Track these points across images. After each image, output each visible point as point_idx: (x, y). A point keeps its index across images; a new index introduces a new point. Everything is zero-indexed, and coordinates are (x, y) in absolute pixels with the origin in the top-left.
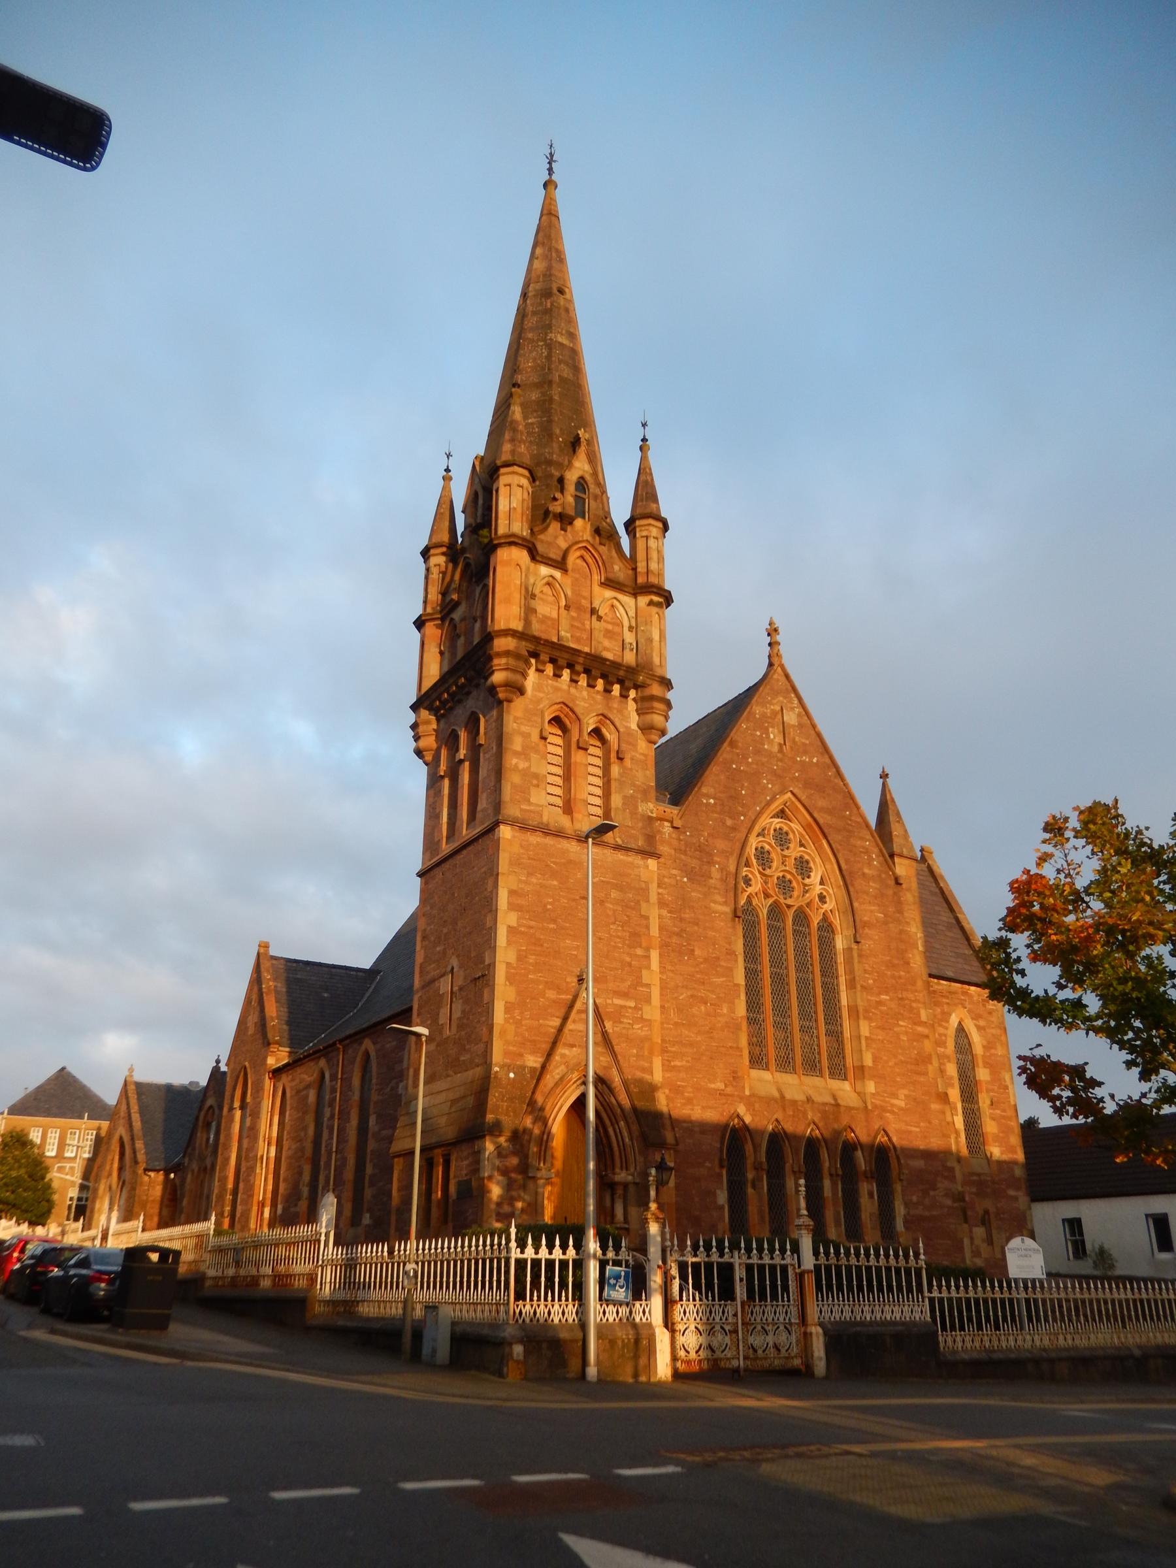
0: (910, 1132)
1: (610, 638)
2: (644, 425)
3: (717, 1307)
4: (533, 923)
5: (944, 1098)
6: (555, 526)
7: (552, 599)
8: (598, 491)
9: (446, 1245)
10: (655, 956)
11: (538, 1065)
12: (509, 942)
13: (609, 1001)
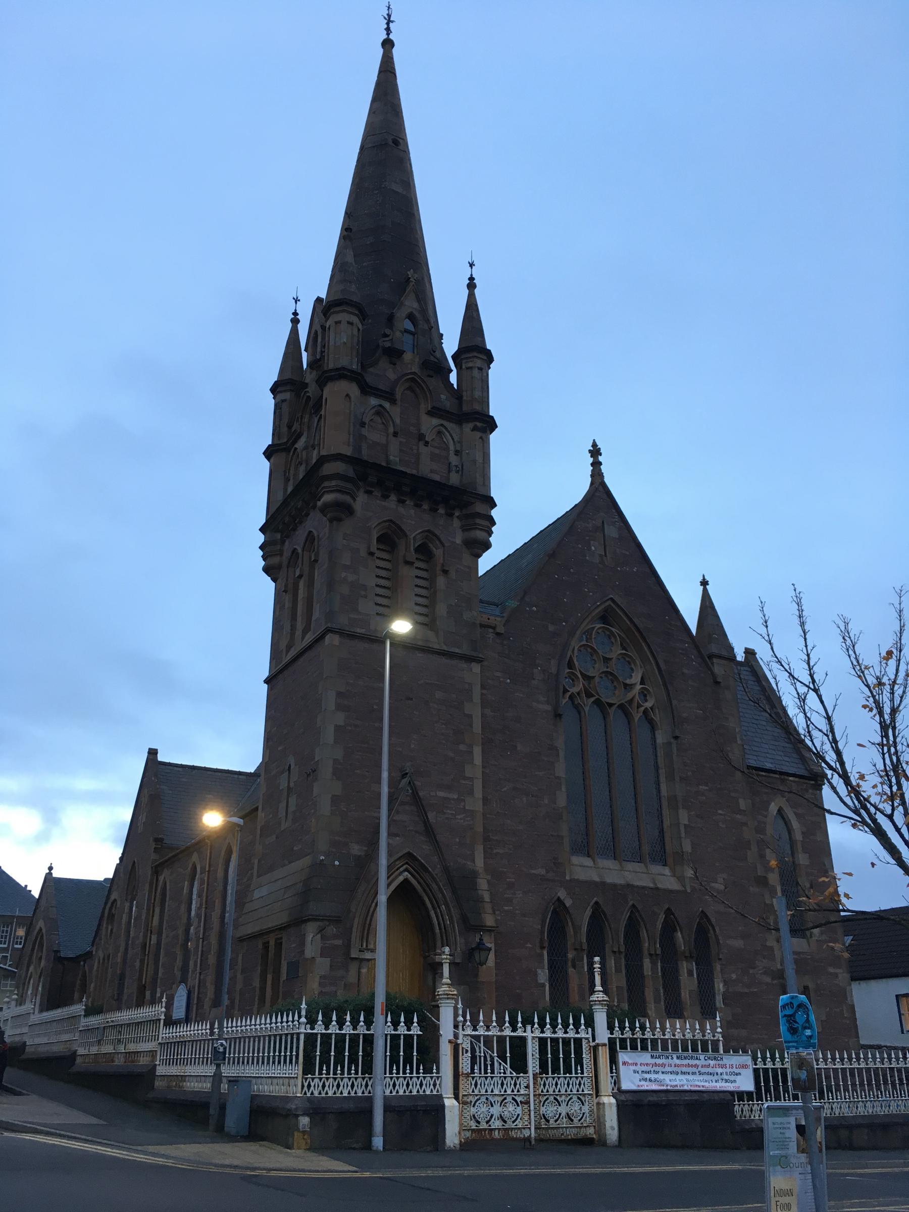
2: (471, 265)
5: (763, 882)
8: (426, 327)
10: (477, 751)
13: (433, 794)
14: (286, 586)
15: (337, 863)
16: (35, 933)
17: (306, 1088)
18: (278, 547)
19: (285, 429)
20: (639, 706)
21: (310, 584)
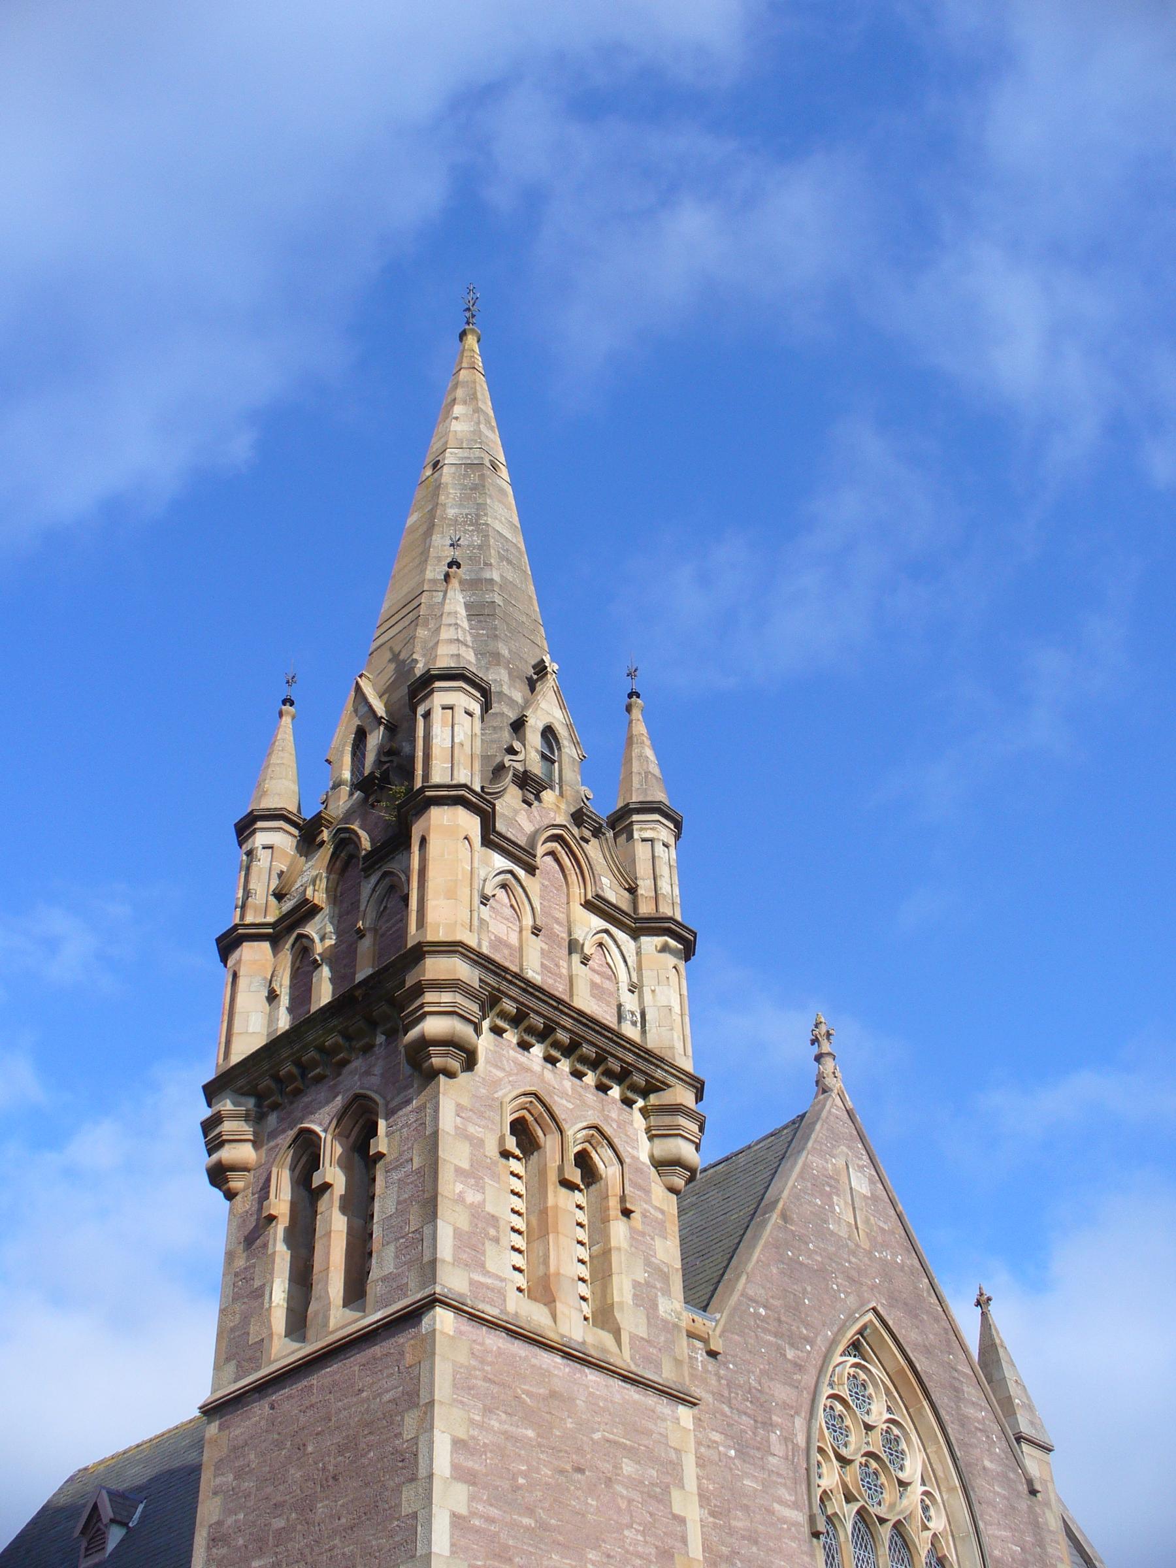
4: (494, 1512)
7: (510, 912)
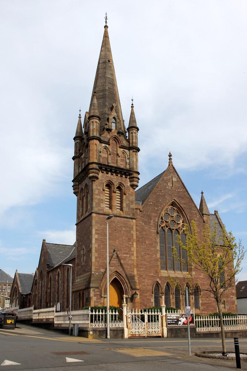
0: (204, 283)
1: (122, 162)
2: (132, 100)
3: (150, 324)
4: (102, 237)
6: (106, 133)
7: (106, 152)
9: (84, 311)
10: (135, 244)
11: (104, 271)
12: (96, 242)
13: (122, 255)
14: (80, 198)
15: (97, 274)
16: (14, 288)
17: (91, 326)
18: (77, 187)
19: (78, 151)
20: (181, 229)
21: (87, 198)
